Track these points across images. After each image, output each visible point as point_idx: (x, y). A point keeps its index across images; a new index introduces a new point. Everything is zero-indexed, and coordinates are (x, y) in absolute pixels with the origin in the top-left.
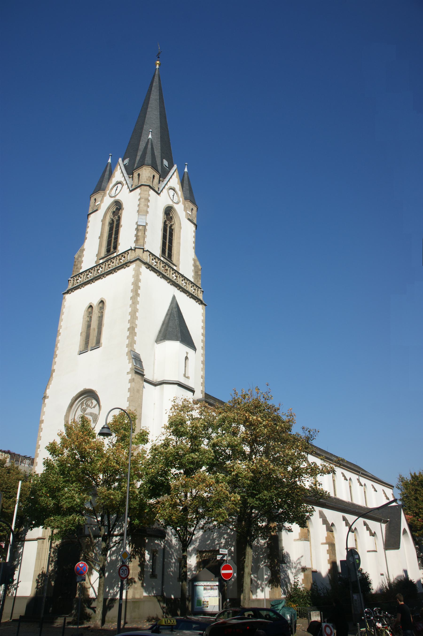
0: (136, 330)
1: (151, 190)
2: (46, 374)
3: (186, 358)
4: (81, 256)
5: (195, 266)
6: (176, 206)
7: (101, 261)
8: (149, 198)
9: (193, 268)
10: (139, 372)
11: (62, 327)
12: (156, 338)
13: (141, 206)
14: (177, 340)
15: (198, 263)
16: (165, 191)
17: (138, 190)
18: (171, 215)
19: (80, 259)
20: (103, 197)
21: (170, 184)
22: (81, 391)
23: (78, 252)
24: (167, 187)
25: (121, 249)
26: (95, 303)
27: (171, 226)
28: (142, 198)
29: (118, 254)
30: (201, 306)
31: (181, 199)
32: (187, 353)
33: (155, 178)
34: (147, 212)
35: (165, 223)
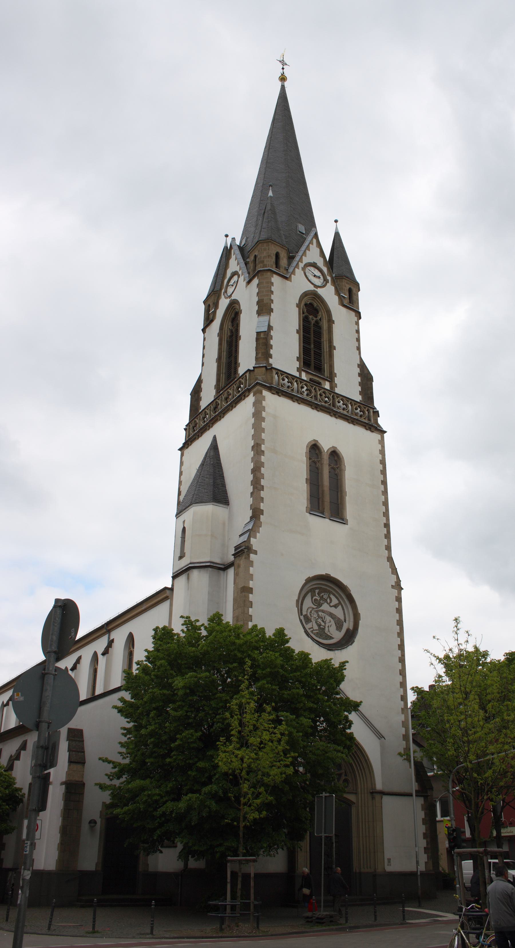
16: (299, 272)
24: (301, 265)
25: (241, 371)
31: (329, 278)
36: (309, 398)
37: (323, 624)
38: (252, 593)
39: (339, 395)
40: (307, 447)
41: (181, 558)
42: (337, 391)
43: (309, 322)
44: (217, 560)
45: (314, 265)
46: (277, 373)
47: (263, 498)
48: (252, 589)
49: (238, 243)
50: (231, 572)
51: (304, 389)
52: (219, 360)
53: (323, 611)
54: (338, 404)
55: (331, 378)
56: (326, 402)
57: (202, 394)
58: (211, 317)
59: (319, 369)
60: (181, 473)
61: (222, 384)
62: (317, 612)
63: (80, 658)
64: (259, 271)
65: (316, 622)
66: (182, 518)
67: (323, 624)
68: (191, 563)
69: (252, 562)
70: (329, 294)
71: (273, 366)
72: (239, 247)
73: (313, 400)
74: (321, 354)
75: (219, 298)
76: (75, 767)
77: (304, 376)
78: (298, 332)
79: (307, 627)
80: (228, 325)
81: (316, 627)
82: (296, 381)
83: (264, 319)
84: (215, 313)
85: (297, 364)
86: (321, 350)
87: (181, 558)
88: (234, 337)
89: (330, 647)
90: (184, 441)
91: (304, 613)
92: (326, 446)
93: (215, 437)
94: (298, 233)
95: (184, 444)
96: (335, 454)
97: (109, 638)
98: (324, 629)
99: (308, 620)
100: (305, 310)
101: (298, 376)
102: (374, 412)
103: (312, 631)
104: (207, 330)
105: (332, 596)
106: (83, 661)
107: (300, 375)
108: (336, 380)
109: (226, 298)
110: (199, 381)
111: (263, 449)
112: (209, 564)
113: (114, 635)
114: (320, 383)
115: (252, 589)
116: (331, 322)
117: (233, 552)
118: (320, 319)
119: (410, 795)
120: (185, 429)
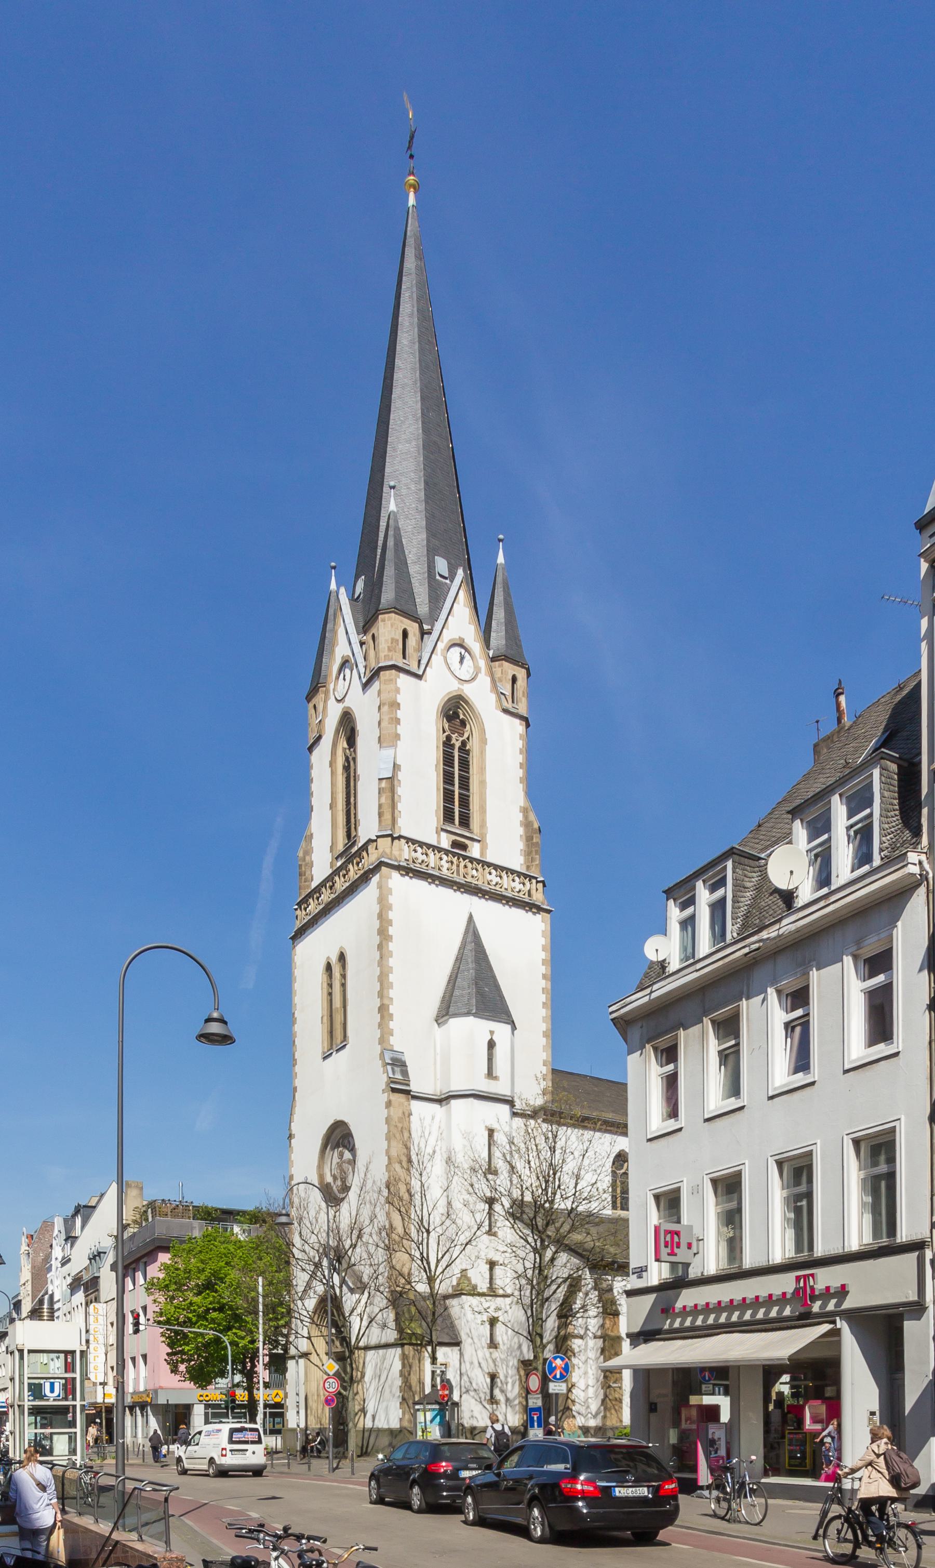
0: (392, 1009)
1: (402, 675)
2: (287, 1095)
3: (491, 1045)
4: (309, 852)
5: (527, 824)
6: (468, 691)
7: (339, 864)
8: (399, 699)
9: (521, 831)
10: (400, 1089)
11: (298, 1007)
12: (436, 1013)
13: (383, 724)
14: (468, 1014)
15: (532, 817)
16: (437, 659)
17: (376, 685)
18: (462, 717)
19: (307, 858)
20: (325, 702)
21: (448, 636)
22: (333, 1124)
23: (303, 844)
24: (441, 646)
26: (334, 959)
27: (464, 744)
28: (384, 704)
29: (360, 845)
30: (539, 917)
32: (492, 1033)
33: (410, 636)
34: (397, 737)
35: (448, 743)
43: (452, 746)
59: (465, 822)
74: (469, 796)
83: (388, 753)
86: (468, 807)
94: (438, 577)
116: (484, 741)
118: (468, 738)
119: (30, 1351)
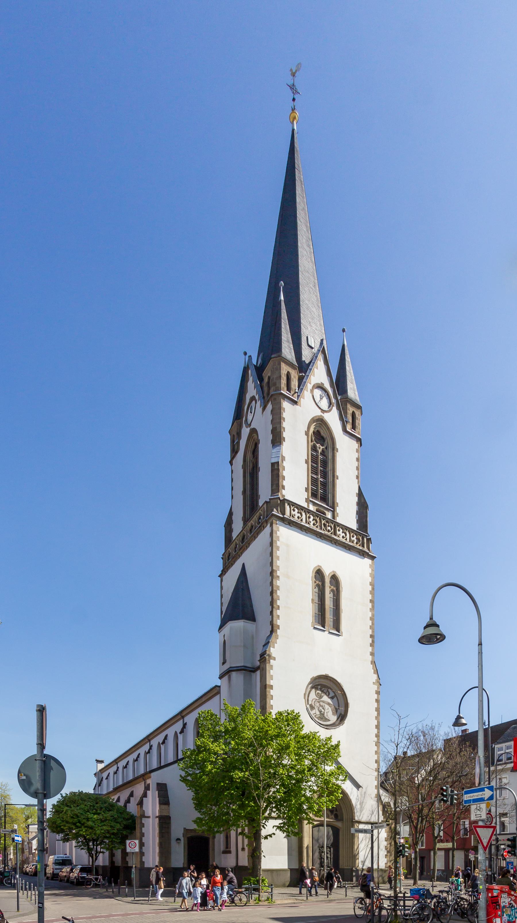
6: (327, 417)
16: (307, 394)
24: (309, 386)
25: (261, 503)
31: (333, 401)
36: (314, 528)
37: (323, 711)
38: (272, 689)
39: (339, 525)
40: (313, 572)
41: (224, 663)
42: (339, 520)
43: (316, 451)
44: (249, 665)
45: (320, 387)
46: (289, 504)
47: (279, 616)
48: (272, 686)
49: (254, 362)
50: (258, 673)
51: (311, 519)
52: (244, 492)
53: (323, 702)
54: (338, 533)
55: (333, 507)
56: (329, 531)
57: (234, 526)
58: (236, 447)
60: (222, 596)
61: (248, 516)
62: (319, 702)
63: (167, 736)
64: (272, 395)
65: (318, 709)
66: (222, 633)
67: (323, 711)
68: (230, 667)
69: (272, 666)
70: (333, 419)
71: (286, 498)
72: (256, 367)
73: (318, 530)
75: (240, 427)
76: (164, 807)
77: (312, 508)
78: (307, 462)
79: (312, 713)
80: (249, 455)
81: (318, 713)
82: (305, 512)
84: (238, 443)
85: (305, 495)
87: (224, 663)
88: (255, 468)
89: (327, 727)
90: (222, 569)
91: (310, 703)
92: (327, 572)
93: (244, 564)
95: (222, 571)
96: (335, 579)
97: (183, 722)
98: (323, 714)
99: (312, 707)
100: (313, 438)
101: (306, 507)
102: (367, 539)
103: (315, 716)
104: (234, 461)
105: (329, 690)
106: (169, 737)
107: (308, 506)
108: (338, 510)
109: (247, 427)
110: (231, 514)
111: (278, 575)
112: (243, 668)
113: (186, 719)
114: (324, 514)
115: (272, 686)
117: (259, 659)
120: (222, 558)
